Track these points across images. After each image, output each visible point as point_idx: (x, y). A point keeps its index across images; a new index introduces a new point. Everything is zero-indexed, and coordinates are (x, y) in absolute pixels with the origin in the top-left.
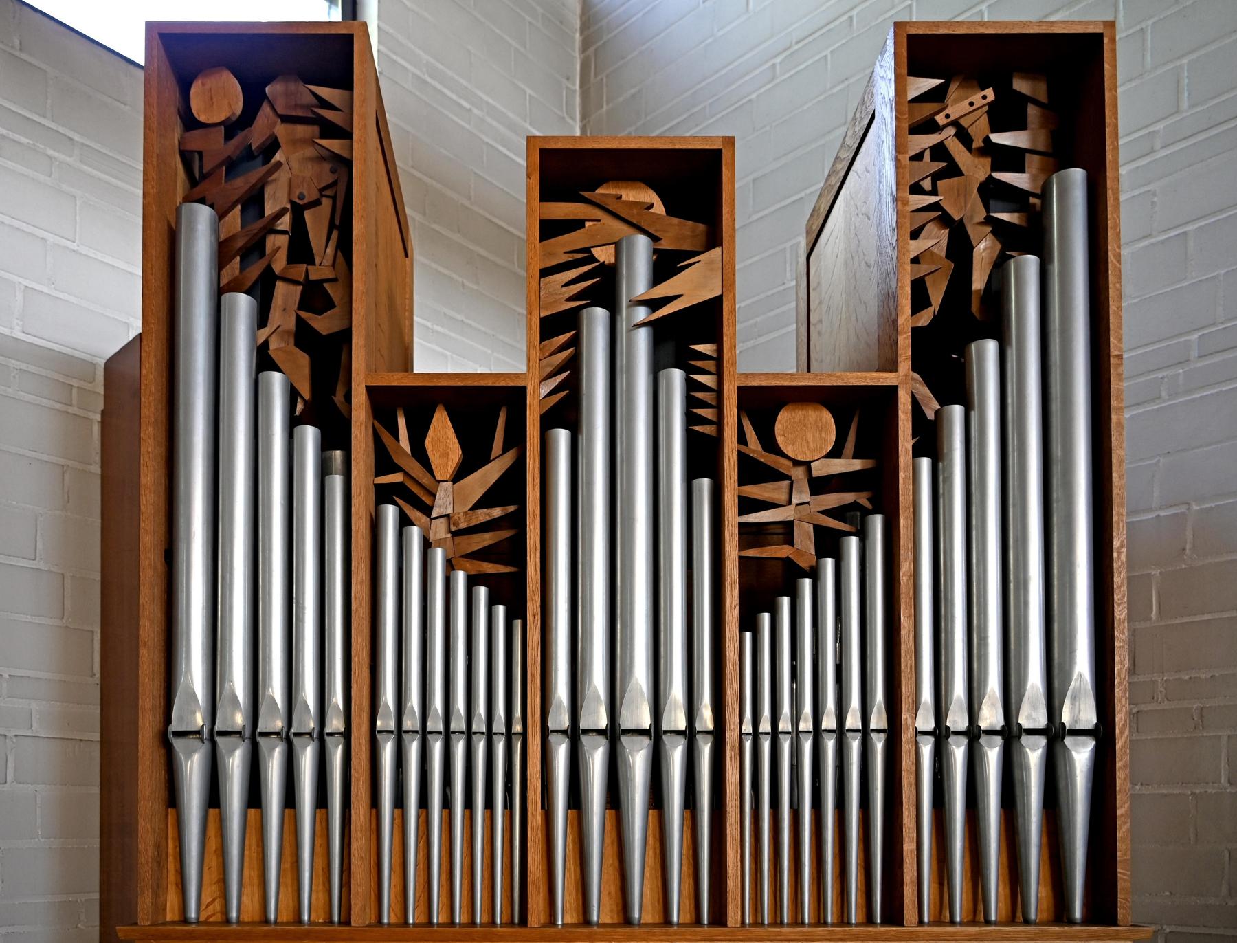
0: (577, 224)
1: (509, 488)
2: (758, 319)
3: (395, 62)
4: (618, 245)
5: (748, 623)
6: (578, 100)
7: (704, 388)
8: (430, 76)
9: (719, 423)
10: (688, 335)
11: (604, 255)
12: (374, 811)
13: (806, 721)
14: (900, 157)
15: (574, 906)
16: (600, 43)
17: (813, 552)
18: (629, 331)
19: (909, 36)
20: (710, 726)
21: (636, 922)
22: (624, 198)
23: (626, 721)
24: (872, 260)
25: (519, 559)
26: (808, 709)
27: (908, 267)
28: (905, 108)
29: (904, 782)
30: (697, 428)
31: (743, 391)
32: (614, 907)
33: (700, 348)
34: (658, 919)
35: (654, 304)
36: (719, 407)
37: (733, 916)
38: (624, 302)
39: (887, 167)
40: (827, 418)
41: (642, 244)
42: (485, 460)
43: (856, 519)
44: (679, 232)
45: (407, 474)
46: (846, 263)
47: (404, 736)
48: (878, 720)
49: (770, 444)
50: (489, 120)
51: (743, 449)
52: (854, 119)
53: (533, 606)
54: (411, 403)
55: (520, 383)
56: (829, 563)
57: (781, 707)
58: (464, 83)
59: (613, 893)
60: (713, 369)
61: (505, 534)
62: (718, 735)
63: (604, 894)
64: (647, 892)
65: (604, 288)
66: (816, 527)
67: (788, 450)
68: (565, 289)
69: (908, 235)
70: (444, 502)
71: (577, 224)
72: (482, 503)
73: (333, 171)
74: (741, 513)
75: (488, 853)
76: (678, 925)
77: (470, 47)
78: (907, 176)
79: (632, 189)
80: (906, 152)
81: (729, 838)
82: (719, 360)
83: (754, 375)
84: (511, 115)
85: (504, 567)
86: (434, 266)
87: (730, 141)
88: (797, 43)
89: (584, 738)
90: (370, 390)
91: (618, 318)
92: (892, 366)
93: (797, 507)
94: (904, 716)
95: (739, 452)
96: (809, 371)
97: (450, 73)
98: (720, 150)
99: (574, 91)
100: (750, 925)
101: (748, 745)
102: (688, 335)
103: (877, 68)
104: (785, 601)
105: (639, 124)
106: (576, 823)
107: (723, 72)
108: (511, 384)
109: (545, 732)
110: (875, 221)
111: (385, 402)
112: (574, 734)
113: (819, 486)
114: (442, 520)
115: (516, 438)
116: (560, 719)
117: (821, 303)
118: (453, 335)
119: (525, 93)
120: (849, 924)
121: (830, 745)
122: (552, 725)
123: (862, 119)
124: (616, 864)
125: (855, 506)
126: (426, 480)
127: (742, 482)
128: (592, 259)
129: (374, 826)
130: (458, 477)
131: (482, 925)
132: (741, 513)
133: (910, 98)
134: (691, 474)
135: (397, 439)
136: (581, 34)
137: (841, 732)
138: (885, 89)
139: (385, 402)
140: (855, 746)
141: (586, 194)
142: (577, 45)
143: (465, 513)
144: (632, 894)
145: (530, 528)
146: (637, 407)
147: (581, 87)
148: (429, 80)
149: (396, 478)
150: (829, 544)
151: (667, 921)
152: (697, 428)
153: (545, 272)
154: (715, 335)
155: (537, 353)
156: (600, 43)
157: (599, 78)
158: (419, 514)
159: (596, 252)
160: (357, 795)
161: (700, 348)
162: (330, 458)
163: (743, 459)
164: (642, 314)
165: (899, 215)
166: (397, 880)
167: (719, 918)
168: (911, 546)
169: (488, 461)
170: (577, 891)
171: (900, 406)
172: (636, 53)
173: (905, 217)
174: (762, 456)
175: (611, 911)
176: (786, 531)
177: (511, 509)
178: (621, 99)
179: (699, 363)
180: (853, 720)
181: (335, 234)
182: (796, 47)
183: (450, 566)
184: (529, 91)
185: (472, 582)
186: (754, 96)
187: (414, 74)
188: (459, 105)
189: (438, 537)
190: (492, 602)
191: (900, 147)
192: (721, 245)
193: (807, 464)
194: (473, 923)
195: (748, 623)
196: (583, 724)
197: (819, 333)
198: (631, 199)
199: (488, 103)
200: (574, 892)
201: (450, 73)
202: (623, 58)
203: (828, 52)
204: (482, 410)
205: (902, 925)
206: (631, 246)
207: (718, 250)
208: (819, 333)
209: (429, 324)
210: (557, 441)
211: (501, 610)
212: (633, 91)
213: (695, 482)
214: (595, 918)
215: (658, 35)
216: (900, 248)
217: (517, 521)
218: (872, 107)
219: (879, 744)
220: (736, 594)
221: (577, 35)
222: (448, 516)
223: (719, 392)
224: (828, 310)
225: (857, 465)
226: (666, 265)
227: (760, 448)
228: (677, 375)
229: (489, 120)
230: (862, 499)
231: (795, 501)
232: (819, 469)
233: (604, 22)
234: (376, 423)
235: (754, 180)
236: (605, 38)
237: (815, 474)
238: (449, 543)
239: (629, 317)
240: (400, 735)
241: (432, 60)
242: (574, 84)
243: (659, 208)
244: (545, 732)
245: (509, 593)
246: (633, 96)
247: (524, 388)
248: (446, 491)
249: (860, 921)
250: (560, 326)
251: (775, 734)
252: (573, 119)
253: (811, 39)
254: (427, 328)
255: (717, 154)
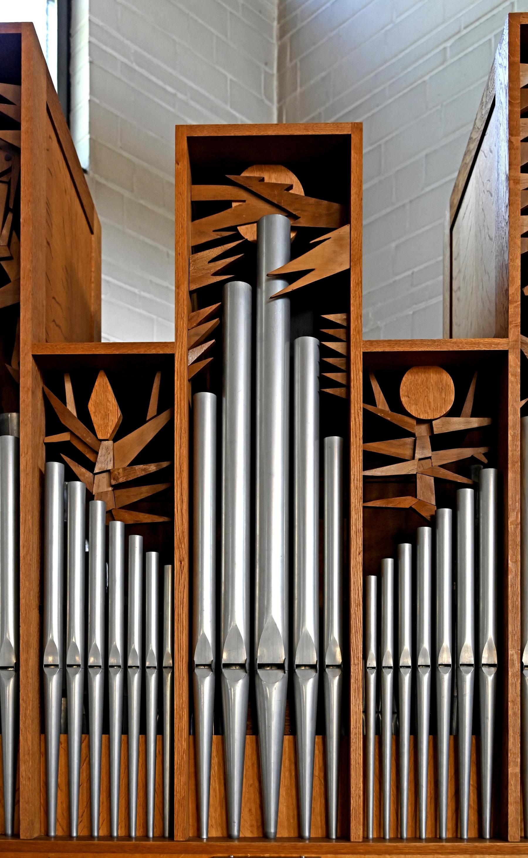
0: (226, 205)
1: (160, 448)
2: (429, 283)
3: (105, 52)
4: (258, 223)
5: (373, 567)
6: (275, 83)
7: (334, 354)
8: (138, 64)
9: (348, 387)
10: (321, 306)
11: (248, 233)
12: (43, 736)
13: (425, 657)
14: (513, 139)
15: (219, 821)
16: (294, 30)
17: (434, 503)
18: (268, 302)
19: (522, 25)
20: (339, 659)
21: (272, 836)
22: (267, 180)
23: (263, 655)
24: (493, 234)
25: (169, 510)
26: (426, 644)
27: (519, 241)
28: (518, 94)
29: (510, 712)
30: (328, 390)
31: (367, 356)
32: (254, 823)
33: (331, 317)
34: (293, 834)
35: (290, 278)
36: (347, 371)
37: (356, 831)
38: (264, 277)
39: (503, 147)
40: (447, 380)
41: (280, 224)
42: (143, 421)
43: (470, 470)
44: (315, 211)
45: (72, 434)
46: (476, 235)
47: (69, 670)
48: (489, 656)
49: (396, 405)
50: (192, 103)
51: (370, 408)
52: (482, 103)
53: (181, 552)
54: (74, 370)
55: (168, 351)
56: (447, 513)
57: (403, 644)
58: (170, 70)
59: (253, 810)
60: (343, 337)
61: (160, 487)
62: (345, 668)
63: (245, 812)
64: (283, 808)
65: (246, 263)
66: (437, 480)
67: (412, 410)
68: (212, 264)
69: (519, 212)
70: (104, 460)
71: (226, 205)
72: (139, 460)
73: (8, 159)
74: (365, 468)
75: (142, 774)
76: (310, 839)
77: (174, 37)
78: (519, 158)
79: (274, 171)
80: (518, 135)
81: (353, 762)
82: (348, 328)
83: (378, 342)
84: (212, 97)
85: (154, 516)
86: (141, 237)
87: (358, 127)
88: (465, 28)
89: (260, 672)
90: (37, 358)
91: (259, 290)
92: (503, 333)
93: (419, 462)
94: (510, 652)
95: (365, 410)
96: (451, 337)
97: (155, 60)
98: (349, 136)
99: (272, 75)
100: (374, 840)
101: (372, 677)
102: (321, 306)
103: (497, 56)
104: (407, 548)
105: (328, 105)
106: (220, 748)
107: (401, 56)
108: (161, 352)
109: (191, 666)
110: (496, 198)
111: (52, 369)
112: (218, 668)
113: (440, 442)
114: (104, 475)
115: (167, 402)
116: (205, 654)
117: (459, 271)
118: (158, 300)
119: (226, 77)
120: (461, 839)
121: (446, 678)
122: (197, 660)
123: (487, 103)
124: (257, 784)
125: (472, 459)
126: (89, 439)
127: (367, 439)
128: (238, 236)
129: (43, 749)
130: (118, 435)
131: (136, 838)
132: (365, 468)
133: (522, 86)
134: (324, 431)
135: (65, 403)
136: (279, 22)
137: (455, 666)
138: (502, 76)
139: (52, 369)
140: (468, 679)
141: (232, 177)
142: (275, 32)
143: (124, 469)
144: (269, 812)
145: (177, 482)
146: (275, 370)
147: (279, 70)
148: (136, 68)
149: (64, 437)
150: (447, 496)
151: (300, 837)
152: (328, 390)
153: (197, 249)
154: (344, 307)
155: (184, 323)
156: (294, 30)
157: (294, 62)
158: (83, 470)
159: (242, 230)
160: (25, 723)
161: (331, 317)
162: (7, 420)
163: (369, 418)
164: (279, 286)
165: (511, 193)
166: (62, 797)
167: (344, 834)
168: (518, 497)
169: (144, 422)
170: (222, 807)
171: (510, 369)
172: (324, 40)
173: (516, 195)
174: (389, 415)
175: (252, 826)
176: (407, 484)
177: (165, 464)
178: (312, 82)
179: (330, 332)
180: (467, 656)
181: (10, 216)
182: (464, 32)
183: (110, 516)
184: (230, 76)
185: (129, 531)
186: (427, 78)
187: (122, 62)
188: (165, 90)
189: (101, 490)
190: (146, 549)
191: (512, 130)
192: (350, 223)
193: (429, 422)
194: (110, 837)
195: (373, 567)
196: (68, 662)
197: (458, 299)
198: (273, 181)
199: (191, 88)
200: (219, 809)
201: (155, 60)
202: (314, 44)
203: (491, 36)
204: (140, 375)
205: (506, 840)
206: (270, 224)
207: (346, 228)
208: (458, 299)
209: (136, 291)
210: (203, 404)
211: (153, 555)
212: (323, 74)
213: (327, 439)
214: (235, 833)
215: (344, 22)
216: (512, 223)
217: (167, 476)
218: (493, 92)
219: (489, 678)
220: (360, 541)
221: (275, 24)
222: (108, 471)
223: (347, 357)
224: (464, 279)
225: (475, 423)
226: (301, 242)
227: (387, 408)
228: (311, 342)
229: (192, 103)
230: (478, 452)
231: (418, 456)
232: (439, 428)
233: (298, 11)
234: (47, 390)
235: (427, 156)
236: (299, 26)
237: (436, 431)
238: (110, 497)
239: (268, 289)
240: (65, 669)
241: (139, 50)
242: (271, 68)
243: (298, 189)
244: (191, 666)
245: (159, 540)
246: (323, 79)
247: (172, 356)
248: (107, 448)
249: (450, 836)
250: (206, 300)
251: (396, 668)
252: (271, 101)
253: (477, 24)
254: (135, 294)
255: (347, 138)
